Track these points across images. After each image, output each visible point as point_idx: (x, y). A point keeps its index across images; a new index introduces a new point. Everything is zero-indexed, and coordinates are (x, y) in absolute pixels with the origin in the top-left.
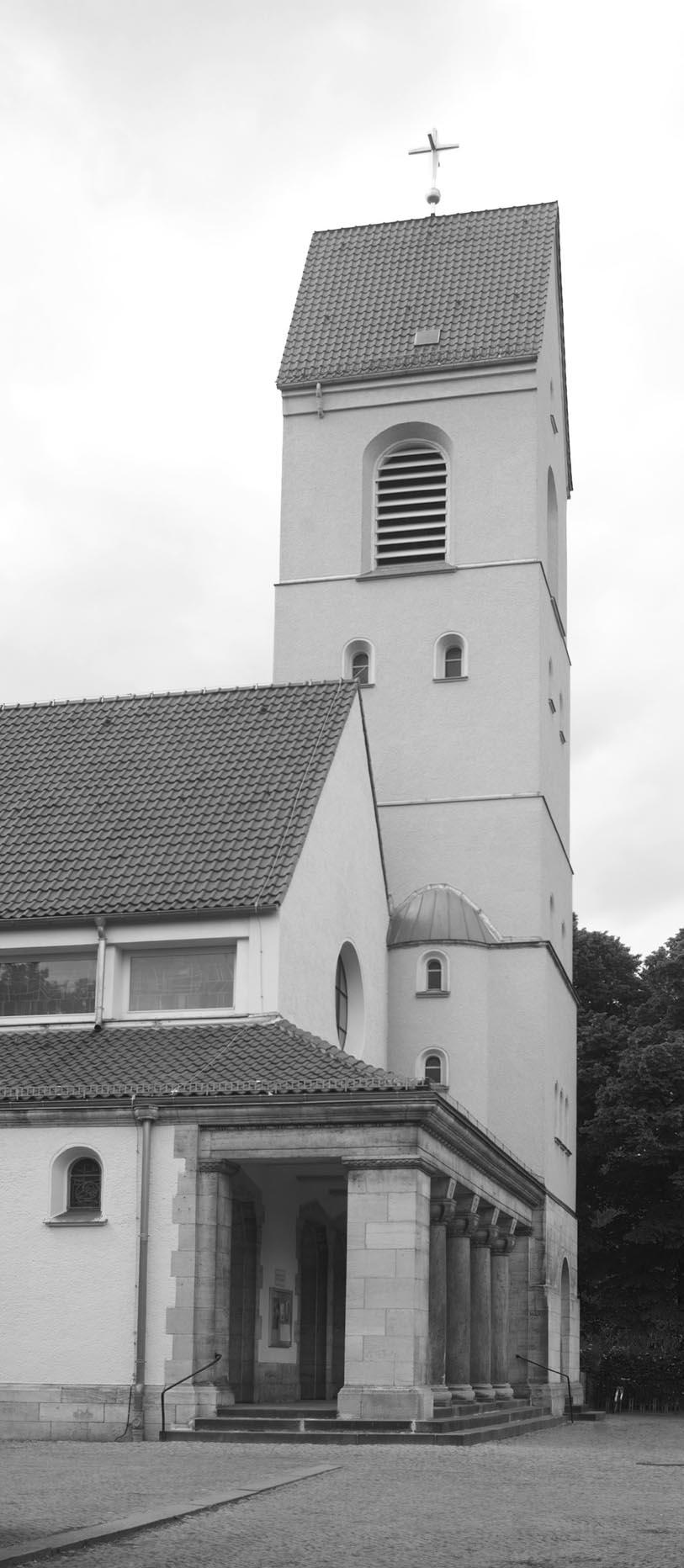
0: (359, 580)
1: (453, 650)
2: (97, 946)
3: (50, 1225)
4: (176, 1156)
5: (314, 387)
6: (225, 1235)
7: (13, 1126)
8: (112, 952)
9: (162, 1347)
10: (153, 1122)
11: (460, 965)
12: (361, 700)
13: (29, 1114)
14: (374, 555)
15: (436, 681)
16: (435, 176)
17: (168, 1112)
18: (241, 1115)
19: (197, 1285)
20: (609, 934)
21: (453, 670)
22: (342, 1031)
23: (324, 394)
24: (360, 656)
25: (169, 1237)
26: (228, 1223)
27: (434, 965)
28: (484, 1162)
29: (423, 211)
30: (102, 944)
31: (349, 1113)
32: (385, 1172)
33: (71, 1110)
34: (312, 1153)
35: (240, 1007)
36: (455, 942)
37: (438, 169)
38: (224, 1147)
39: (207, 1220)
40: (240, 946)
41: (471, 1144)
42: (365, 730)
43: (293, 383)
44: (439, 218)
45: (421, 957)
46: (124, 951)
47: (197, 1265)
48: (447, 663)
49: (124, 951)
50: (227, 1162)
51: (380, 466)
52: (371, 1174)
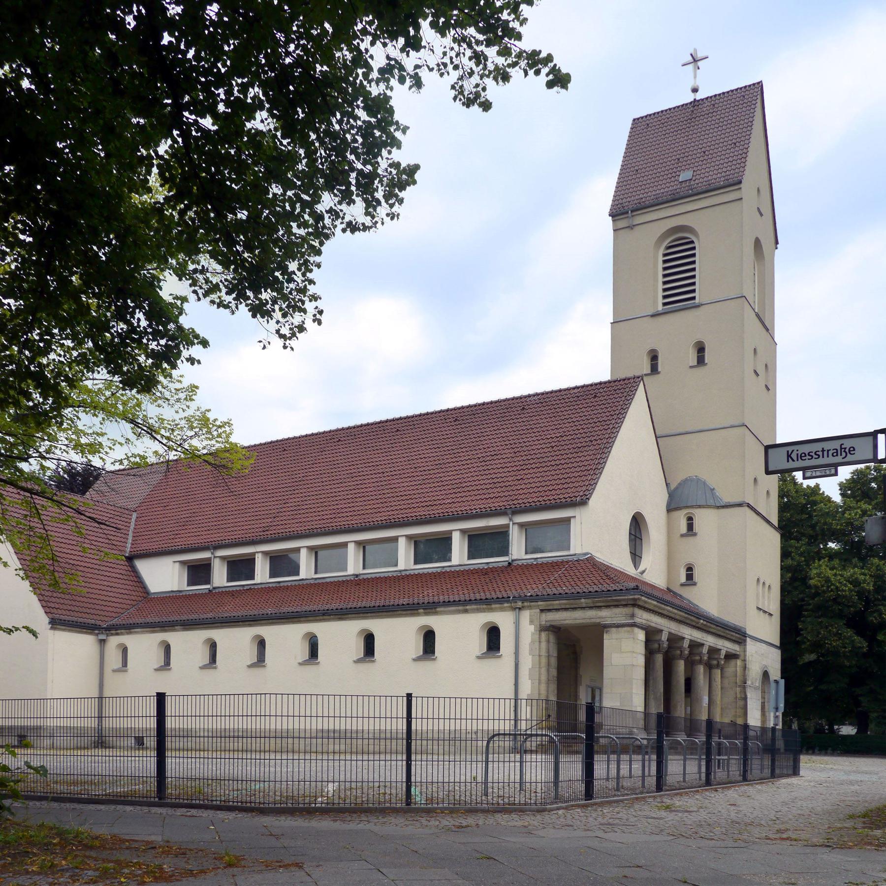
0: (652, 316)
1: (701, 349)
2: (509, 524)
3: (478, 658)
4: (530, 624)
5: (628, 212)
6: (554, 661)
7: (463, 613)
8: (516, 527)
9: (525, 712)
10: (520, 609)
11: (705, 519)
12: (644, 385)
13: (438, 609)
14: (661, 301)
15: (691, 367)
16: (695, 77)
17: (526, 604)
18: (557, 604)
19: (539, 683)
20: (31, 589)
21: (701, 361)
22: (636, 556)
23: (632, 216)
24: (654, 357)
25: (527, 662)
26: (555, 654)
27: (690, 519)
28: (688, 621)
29: (689, 98)
30: (511, 523)
31: (603, 602)
32: (620, 629)
33: (487, 603)
34: (588, 621)
35: (303, 575)
36: (700, 507)
37: (698, 71)
38: (551, 619)
39: (544, 653)
40: (572, 520)
41: (675, 614)
42: (648, 400)
43: (615, 214)
44: (699, 101)
45: (682, 516)
46: (522, 525)
47: (540, 674)
48: (698, 356)
49: (522, 525)
50: (553, 626)
51: (662, 251)
52: (614, 630)
